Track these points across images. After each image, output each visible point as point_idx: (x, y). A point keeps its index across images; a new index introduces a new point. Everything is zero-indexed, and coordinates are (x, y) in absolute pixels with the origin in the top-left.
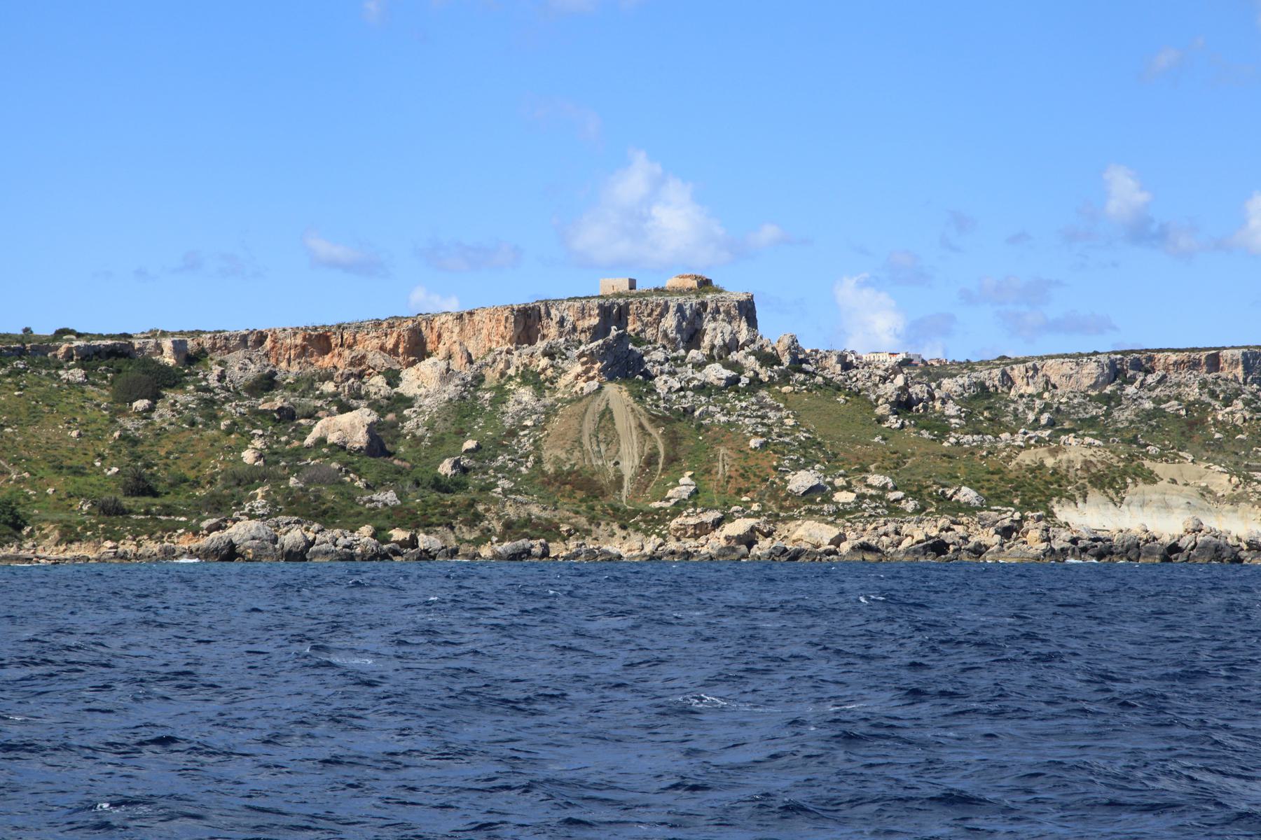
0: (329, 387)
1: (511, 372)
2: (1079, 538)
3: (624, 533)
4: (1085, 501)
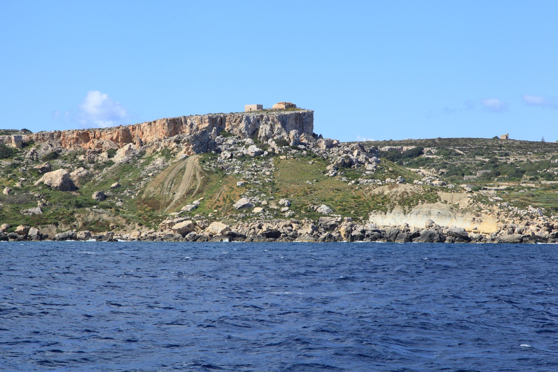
0: (81, 158)
1: (158, 150)
2: (366, 230)
3: (139, 228)
4: (391, 212)
